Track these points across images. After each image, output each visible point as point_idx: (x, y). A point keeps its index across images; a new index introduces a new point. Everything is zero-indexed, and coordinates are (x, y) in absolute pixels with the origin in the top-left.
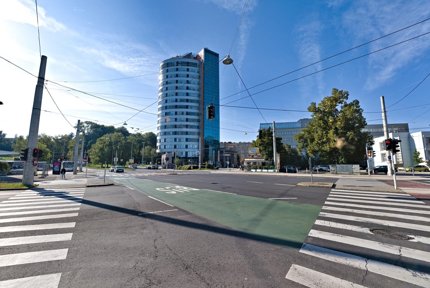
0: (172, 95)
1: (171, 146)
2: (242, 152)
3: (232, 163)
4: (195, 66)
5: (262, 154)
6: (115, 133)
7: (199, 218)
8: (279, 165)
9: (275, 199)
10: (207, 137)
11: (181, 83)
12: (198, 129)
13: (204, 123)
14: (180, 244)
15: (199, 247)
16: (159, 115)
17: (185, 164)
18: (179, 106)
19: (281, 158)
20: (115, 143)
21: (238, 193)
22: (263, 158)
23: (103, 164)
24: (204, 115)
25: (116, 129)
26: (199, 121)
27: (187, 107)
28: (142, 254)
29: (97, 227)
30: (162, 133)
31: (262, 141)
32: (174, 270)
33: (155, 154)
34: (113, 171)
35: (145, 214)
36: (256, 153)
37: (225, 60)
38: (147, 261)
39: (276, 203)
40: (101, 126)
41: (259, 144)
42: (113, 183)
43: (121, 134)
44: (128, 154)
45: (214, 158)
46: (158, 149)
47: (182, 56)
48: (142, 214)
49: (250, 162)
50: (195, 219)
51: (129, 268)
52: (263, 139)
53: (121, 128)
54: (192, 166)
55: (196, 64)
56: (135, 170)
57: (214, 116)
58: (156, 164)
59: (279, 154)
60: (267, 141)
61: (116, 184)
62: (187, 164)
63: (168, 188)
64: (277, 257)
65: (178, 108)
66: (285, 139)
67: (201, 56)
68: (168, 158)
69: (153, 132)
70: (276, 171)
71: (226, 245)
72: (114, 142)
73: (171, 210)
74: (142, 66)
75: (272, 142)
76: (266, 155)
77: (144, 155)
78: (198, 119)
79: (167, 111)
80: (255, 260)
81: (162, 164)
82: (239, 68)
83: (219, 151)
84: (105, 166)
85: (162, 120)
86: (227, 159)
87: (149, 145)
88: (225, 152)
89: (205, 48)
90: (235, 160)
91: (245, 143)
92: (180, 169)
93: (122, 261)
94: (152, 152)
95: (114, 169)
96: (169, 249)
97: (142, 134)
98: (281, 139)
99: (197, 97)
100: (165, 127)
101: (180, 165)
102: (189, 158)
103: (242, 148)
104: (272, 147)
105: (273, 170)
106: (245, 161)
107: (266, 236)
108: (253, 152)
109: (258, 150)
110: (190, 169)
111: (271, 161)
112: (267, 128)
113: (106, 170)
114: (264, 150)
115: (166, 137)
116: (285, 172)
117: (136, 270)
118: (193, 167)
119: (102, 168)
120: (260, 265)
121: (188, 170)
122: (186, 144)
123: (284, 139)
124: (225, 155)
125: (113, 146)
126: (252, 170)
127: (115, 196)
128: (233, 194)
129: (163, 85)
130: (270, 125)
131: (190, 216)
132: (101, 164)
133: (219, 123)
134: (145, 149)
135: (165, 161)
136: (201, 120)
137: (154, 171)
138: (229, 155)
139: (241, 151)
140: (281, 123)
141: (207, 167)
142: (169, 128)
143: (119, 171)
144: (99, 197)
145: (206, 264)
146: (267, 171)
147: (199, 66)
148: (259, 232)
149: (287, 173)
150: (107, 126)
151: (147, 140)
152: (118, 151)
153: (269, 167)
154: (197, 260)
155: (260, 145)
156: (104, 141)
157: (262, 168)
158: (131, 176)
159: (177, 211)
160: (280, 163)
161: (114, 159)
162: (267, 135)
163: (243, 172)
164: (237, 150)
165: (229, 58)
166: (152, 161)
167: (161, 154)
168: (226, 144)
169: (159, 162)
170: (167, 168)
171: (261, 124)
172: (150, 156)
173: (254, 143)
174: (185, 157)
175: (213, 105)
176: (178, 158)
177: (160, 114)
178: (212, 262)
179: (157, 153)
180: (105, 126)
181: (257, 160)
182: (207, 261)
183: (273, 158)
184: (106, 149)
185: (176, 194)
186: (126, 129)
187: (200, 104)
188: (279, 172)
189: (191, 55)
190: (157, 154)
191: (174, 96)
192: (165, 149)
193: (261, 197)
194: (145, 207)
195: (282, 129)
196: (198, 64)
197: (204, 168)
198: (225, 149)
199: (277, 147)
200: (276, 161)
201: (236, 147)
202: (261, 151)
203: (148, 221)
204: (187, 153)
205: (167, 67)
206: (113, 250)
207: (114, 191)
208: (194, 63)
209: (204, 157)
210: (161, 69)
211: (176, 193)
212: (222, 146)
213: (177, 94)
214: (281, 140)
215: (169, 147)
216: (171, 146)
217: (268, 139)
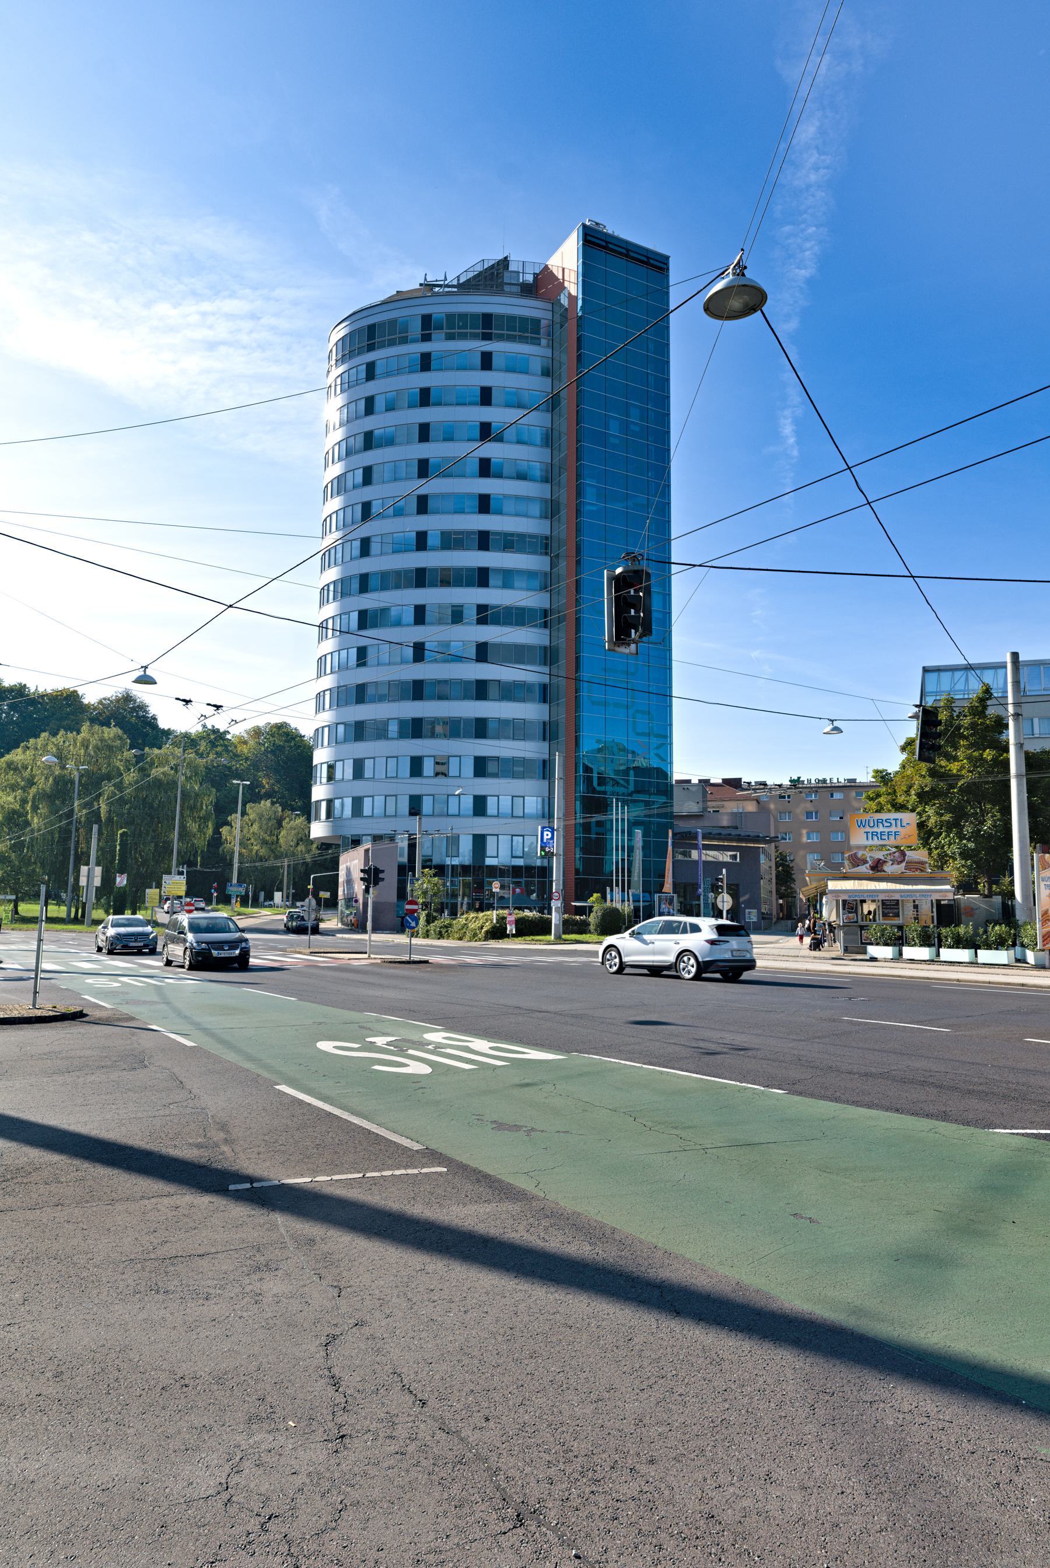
0: (399, 513)
1: (391, 801)
2: (805, 839)
3: (744, 902)
4: (515, 336)
6: (85, 727)
7: (559, 1218)
9: (1035, 1131)
10: (599, 750)
11: (449, 438)
12: (545, 701)
13: (577, 669)
14: (473, 1373)
15: (584, 1396)
16: (322, 626)
18: (434, 570)
21: (793, 1087)
22: (939, 874)
23: (23, 900)
24: (578, 621)
25: (88, 706)
26: (548, 656)
27: (482, 577)
28: (261, 1420)
29: (10, 1253)
30: (341, 729)
31: (933, 773)
32: (445, 1523)
33: (301, 848)
36: (896, 843)
37: (716, 293)
40: (11, 690)
41: (919, 795)
42: (79, 1009)
43: (120, 732)
46: (317, 818)
47: (455, 283)
48: (248, 1186)
51: (195, 1496)
52: (943, 763)
53: (118, 700)
54: (512, 916)
55: (536, 322)
57: (647, 631)
58: (310, 901)
60: (968, 777)
62: (481, 904)
63: (380, 1041)
65: (433, 585)
67: (560, 277)
68: (377, 871)
69: (293, 726)
70: (1030, 956)
71: (746, 1400)
72: (81, 776)
73: (410, 1171)
74: (223, 349)
75: (1000, 777)
76: (959, 862)
77: (240, 854)
78: (545, 648)
79: (371, 601)
80: (934, 1508)
81: (341, 903)
84: (37, 914)
85: (344, 653)
86: (718, 880)
87: (268, 796)
88: (704, 838)
89: (584, 226)
90: (767, 886)
91: (824, 788)
92: (440, 936)
94: (286, 838)
96: (409, 1399)
97: (229, 737)
99: (541, 517)
100: (361, 694)
101: (441, 911)
102: (495, 872)
103: (809, 815)
104: (1000, 811)
105: (1012, 952)
106: (833, 892)
107: (992, 1362)
108: (876, 842)
109: (913, 830)
110: (498, 933)
111: (998, 899)
112: (966, 691)
113: (45, 935)
115: (361, 749)
117: (233, 1510)
119: (17, 926)
121: (486, 939)
122: (356, 757)
124: (704, 858)
126: (873, 950)
127: (93, 1077)
128: (763, 1092)
129: (348, 453)
130: (988, 677)
131: (515, 1208)
132: (10, 901)
133: (670, 669)
134: (246, 818)
135: (359, 887)
137: (299, 944)
138: (725, 857)
139: (804, 832)
141: (597, 926)
142: (381, 699)
144: (10, 1083)
147: (550, 334)
148: (945, 1333)
150: (41, 690)
151: (256, 766)
152: (100, 833)
153: (986, 932)
154: (576, 1475)
155: (924, 797)
156: (26, 774)
157: (940, 941)
159: (440, 1174)
161: (79, 871)
162: (966, 738)
163: (820, 958)
164: (776, 831)
165: (742, 281)
166: (288, 888)
167: (338, 846)
169: (325, 895)
171: (926, 670)
172: (276, 857)
175: (644, 565)
176: (432, 872)
177: (330, 622)
178: (667, 1492)
179: (312, 842)
180: (32, 690)
181: (906, 887)
184: (36, 820)
185: (427, 1075)
186: (143, 707)
187: (557, 556)
189: (506, 274)
190: (315, 846)
191: (407, 515)
192: (358, 821)
193: (944, 1117)
194: (262, 1149)
196: (543, 323)
197: (582, 928)
201: (772, 806)
202: (930, 833)
203: (282, 1230)
204: (480, 841)
205: (371, 348)
206: (103, 1387)
207: (88, 1053)
208: (524, 320)
209: (579, 865)
210: (333, 362)
211: (427, 1070)
212: (684, 805)
213: (423, 505)
215: (379, 811)
216: (391, 801)
217: (976, 762)
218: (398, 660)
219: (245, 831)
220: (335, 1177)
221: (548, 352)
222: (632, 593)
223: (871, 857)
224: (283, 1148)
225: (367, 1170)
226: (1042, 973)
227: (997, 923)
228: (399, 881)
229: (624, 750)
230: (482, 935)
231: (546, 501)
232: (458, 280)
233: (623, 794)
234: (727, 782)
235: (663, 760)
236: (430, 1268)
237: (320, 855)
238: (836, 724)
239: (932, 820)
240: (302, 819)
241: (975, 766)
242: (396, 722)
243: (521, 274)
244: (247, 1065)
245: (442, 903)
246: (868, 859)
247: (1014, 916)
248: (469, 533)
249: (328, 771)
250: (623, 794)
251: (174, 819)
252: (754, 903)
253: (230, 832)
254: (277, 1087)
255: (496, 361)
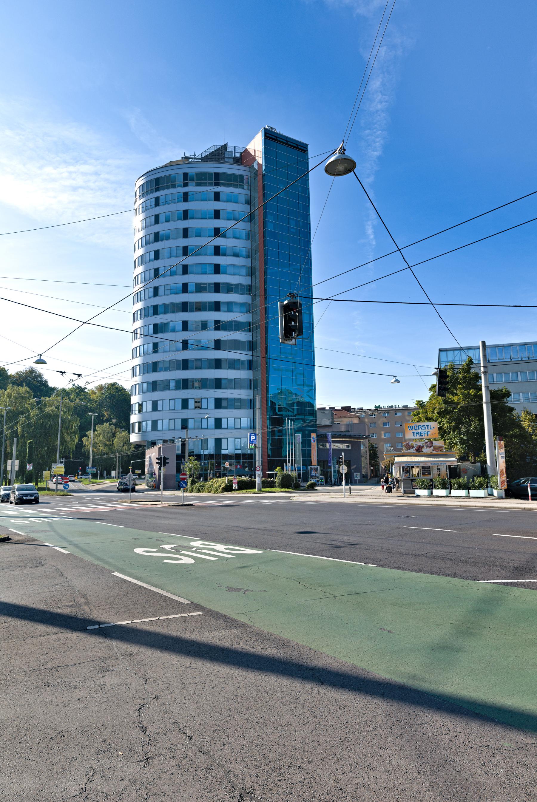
0: (173, 274)
1: (172, 422)
2: (383, 437)
5: (447, 442)
6: (9, 387)
8: (505, 475)
10: (279, 394)
11: (198, 235)
12: (250, 369)
13: (267, 352)
14: (217, 720)
15: (274, 729)
16: (134, 333)
17: (216, 474)
19: (509, 452)
20: (9, 418)
21: (379, 563)
22: (449, 453)
24: (266, 328)
25: (11, 376)
26: (251, 346)
27: (217, 306)
28: (103, 752)
30: (145, 385)
31: (445, 402)
33: (125, 447)
34: (8, 499)
35: (106, 625)
37: (331, 162)
38: (121, 774)
39: (505, 595)
41: (438, 413)
42: (6, 536)
43: (28, 389)
44: (46, 448)
45: (299, 457)
46: (134, 431)
47: (200, 157)
48: (97, 627)
49: (413, 467)
50: (254, 642)
51: (68, 796)
52: (450, 397)
53: (27, 372)
54: (235, 480)
55: (242, 177)
56: (69, 494)
57: (301, 333)
59: (502, 442)
60: (463, 403)
61: (17, 538)
62: (220, 474)
63: (168, 547)
64: (523, 770)
65: (192, 310)
66: (521, 394)
67: (253, 154)
68: (165, 458)
69: (120, 384)
70: (495, 492)
71: (357, 727)
72: (7, 413)
73: (183, 615)
74: (81, 191)
77: (93, 451)
78: (250, 342)
79: (160, 319)
80: (452, 777)
81: (147, 476)
82: (367, 181)
83: (314, 435)
85: (146, 346)
86: (340, 458)
89: (265, 129)
90: (365, 461)
91: (392, 410)
92: (199, 491)
93: (46, 775)
94: (117, 442)
95: (9, 494)
96: (183, 736)
97: (86, 390)
98: (508, 394)
99: (246, 276)
100: (155, 367)
102: (227, 457)
104: (478, 420)
105: (486, 491)
106: (397, 463)
107: (480, 701)
108: (418, 437)
109: (436, 431)
110: (228, 488)
111: (479, 464)
112: (460, 360)
114: (454, 431)
116: (523, 496)
118: (239, 483)
120: (471, 797)
121: (222, 492)
123: (517, 397)
124: (332, 447)
125: (5, 427)
126: (418, 492)
127: (14, 572)
128: (364, 566)
129: (147, 243)
130: (471, 354)
131: (237, 632)
133: (314, 352)
134: (96, 432)
135: (156, 467)
136: (259, 345)
137: (125, 498)
138: (343, 446)
139: (383, 433)
140: (504, 346)
141: (279, 484)
142: (166, 369)
143: (24, 498)
145: (299, 785)
146: (464, 495)
147: (249, 183)
148: (456, 686)
149: (532, 499)
151: (101, 405)
153: (473, 481)
154: (270, 772)
155: (441, 414)
157: (451, 486)
158: (58, 513)
159: (199, 616)
160: (507, 468)
162: (461, 384)
163: (392, 497)
164: (369, 433)
166: (119, 469)
168: (334, 413)
170: (161, 487)
171: (440, 350)
172: (112, 453)
173: (422, 408)
174: (213, 455)
175: (298, 300)
176: (194, 458)
177: (139, 330)
178: (317, 778)
179: (131, 444)
181: (435, 459)
182: (301, 776)
183: (483, 454)
186: (40, 376)
188: (504, 496)
189: (226, 153)
190: (132, 446)
192: (155, 433)
193: (455, 575)
194: (105, 607)
195: (511, 363)
196: (245, 177)
197: (272, 485)
198: (334, 429)
199: (495, 420)
200: (495, 463)
201: (366, 420)
202: (445, 432)
203: (116, 650)
204: (218, 442)
205: (157, 190)
207: (11, 559)
208: (235, 176)
209: (270, 453)
210: (138, 197)
211: (192, 561)
212: (322, 421)
213: (186, 270)
214: (508, 399)
215: (166, 427)
216: (172, 422)
217: (466, 396)
218: (175, 349)
219: (96, 439)
220: (144, 620)
221: (248, 192)
222: (293, 313)
223: (416, 445)
224: (116, 606)
225: (160, 616)
226: (501, 501)
227: (479, 476)
228: (177, 463)
229: (291, 393)
230: (220, 490)
231: (249, 267)
232: (202, 156)
233: (291, 416)
234: (343, 408)
235: (311, 398)
236: (194, 666)
237: (135, 451)
238: (397, 378)
239: (446, 426)
240: (126, 432)
241: (466, 398)
242: (174, 381)
243: (234, 153)
244: (97, 562)
245: (200, 474)
246: (414, 446)
247: (487, 472)
248: (210, 284)
249: (139, 407)
250: (291, 416)
251: (57, 434)
252: (359, 469)
253: (88, 440)
254: (113, 573)
255: (222, 197)
